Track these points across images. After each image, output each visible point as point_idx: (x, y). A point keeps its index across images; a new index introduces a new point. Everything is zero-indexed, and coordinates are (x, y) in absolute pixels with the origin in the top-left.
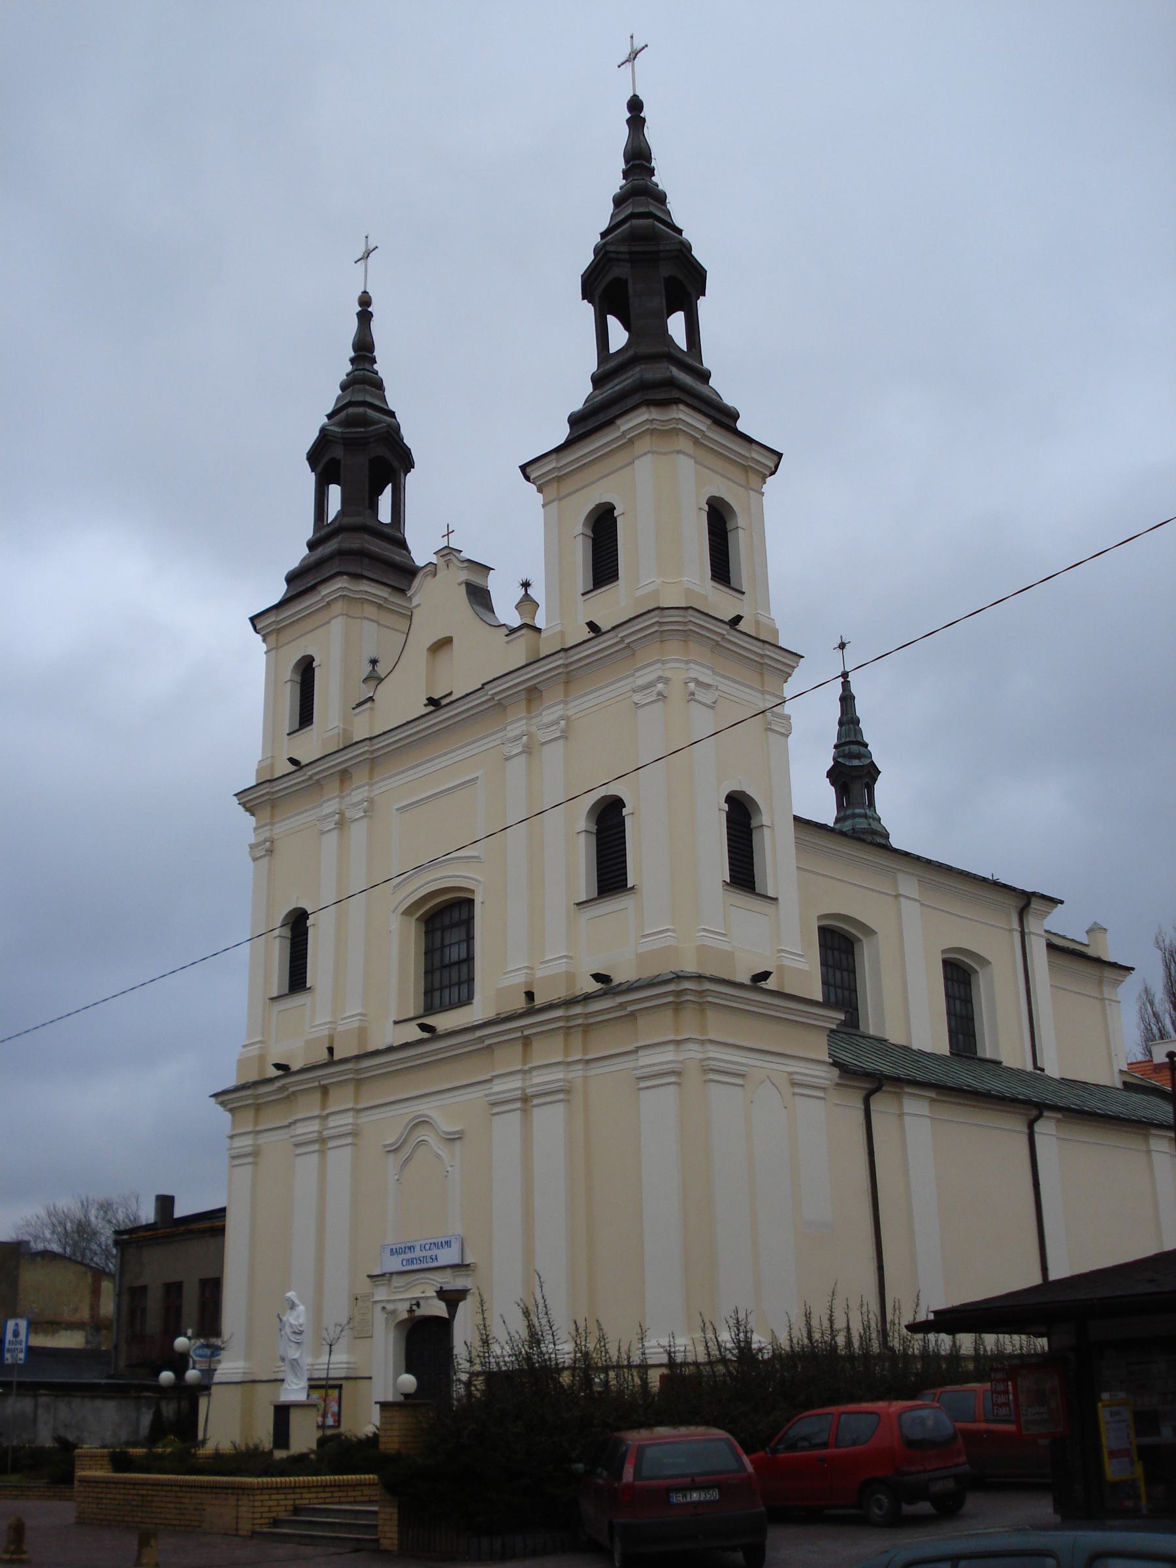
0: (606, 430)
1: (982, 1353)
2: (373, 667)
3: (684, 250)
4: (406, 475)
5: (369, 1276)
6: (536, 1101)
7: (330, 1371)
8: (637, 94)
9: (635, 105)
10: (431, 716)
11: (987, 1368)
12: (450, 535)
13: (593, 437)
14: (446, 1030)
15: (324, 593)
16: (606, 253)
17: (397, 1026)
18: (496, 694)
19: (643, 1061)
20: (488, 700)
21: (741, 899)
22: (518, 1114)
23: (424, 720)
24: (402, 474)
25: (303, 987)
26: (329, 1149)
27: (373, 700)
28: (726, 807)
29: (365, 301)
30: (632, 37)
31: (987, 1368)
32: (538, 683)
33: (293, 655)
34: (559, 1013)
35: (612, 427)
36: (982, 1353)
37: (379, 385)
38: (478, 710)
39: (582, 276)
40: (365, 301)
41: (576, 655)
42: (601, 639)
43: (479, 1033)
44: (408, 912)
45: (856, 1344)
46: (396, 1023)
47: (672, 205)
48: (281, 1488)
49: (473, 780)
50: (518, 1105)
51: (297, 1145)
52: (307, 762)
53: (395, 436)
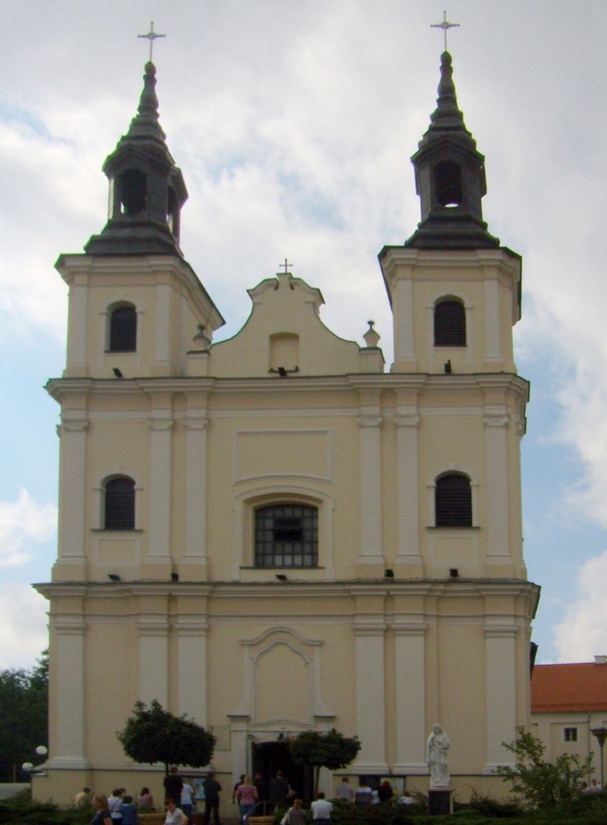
0: (467, 252)
1: (571, 786)
2: (371, 327)
5: (229, 716)
6: (398, 632)
8: (448, 51)
9: (446, 60)
10: (276, 381)
13: (454, 253)
14: (297, 580)
15: (481, 257)
17: (243, 571)
18: (482, 382)
19: (142, 621)
20: (347, 386)
22: (204, 639)
23: (248, 381)
25: (469, 525)
26: (179, 636)
27: (209, 354)
30: (445, 12)
32: (397, 388)
34: (429, 586)
35: (472, 253)
36: (571, 786)
37: (459, 116)
38: (329, 389)
41: (433, 381)
42: (120, 382)
43: (347, 587)
44: (249, 501)
46: (241, 568)
49: (321, 432)
50: (81, 632)
51: (141, 629)
52: (458, 372)
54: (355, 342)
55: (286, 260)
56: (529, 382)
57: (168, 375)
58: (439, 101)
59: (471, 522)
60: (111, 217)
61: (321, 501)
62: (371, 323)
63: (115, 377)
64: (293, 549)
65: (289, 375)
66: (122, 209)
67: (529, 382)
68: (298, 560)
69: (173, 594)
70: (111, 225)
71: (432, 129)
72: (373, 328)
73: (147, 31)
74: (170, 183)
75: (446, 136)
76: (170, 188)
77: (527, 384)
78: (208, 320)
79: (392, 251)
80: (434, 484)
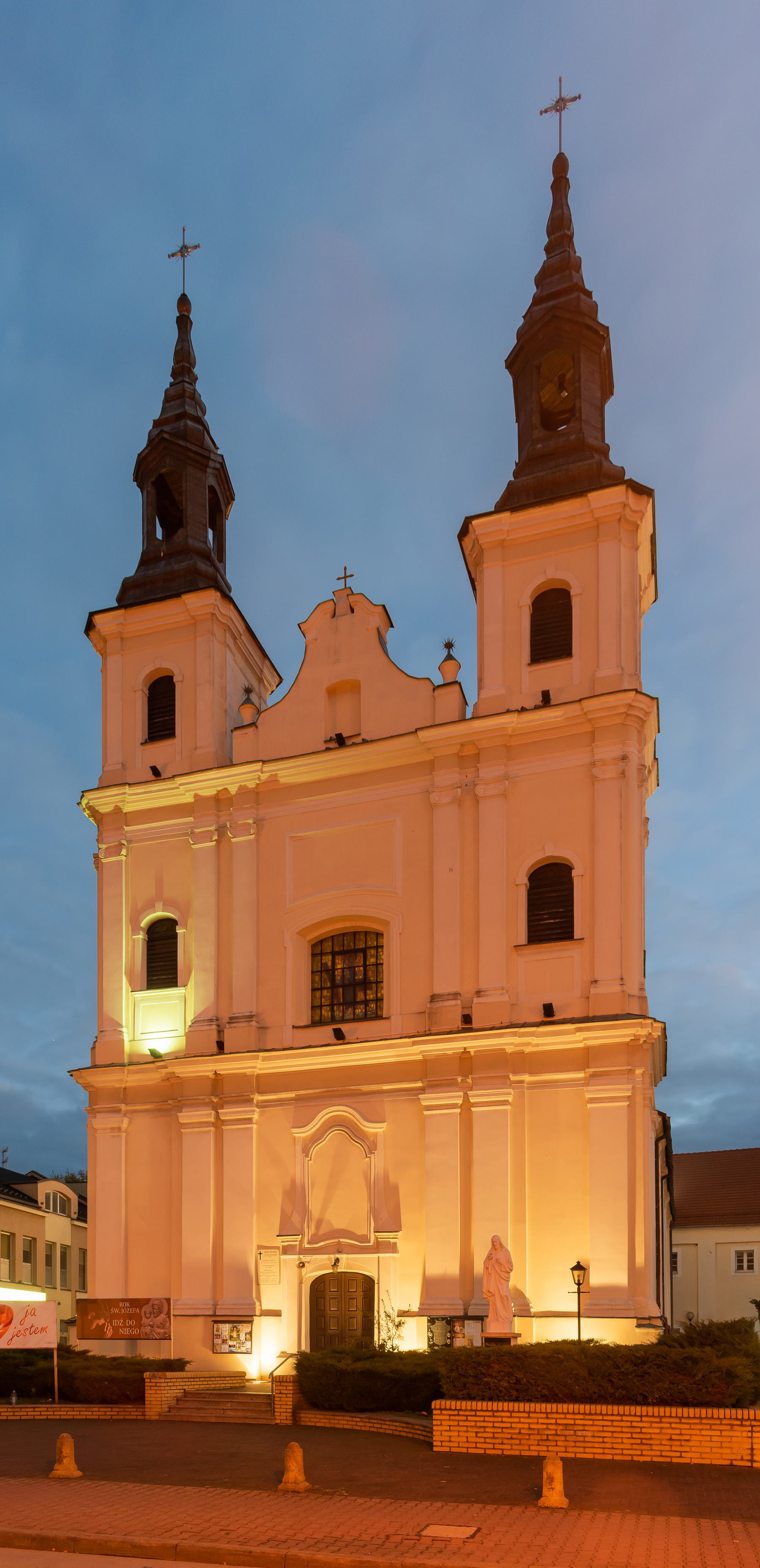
12: (347, 579)
17: (296, 1031)
44: (302, 933)
54: (428, 679)
55: (345, 569)
56: (657, 699)
57: (457, 720)
58: (548, 249)
59: (572, 932)
60: (532, 612)
61: (386, 923)
63: (153, 778)
64: (374, 983)
65: (349, 742)
66: (159, 534)
67: (657, 699)
68: (349, 1013)
69: (218, 1072)
70: (146, 561)
71: (537, 300)
72: (451, 653)
73: (193, 254)
74: (211, 481)
75: (553, 307)
76: (212, 489)
77: (656, 701)
78: (260, 680)
79: (475, 522)
80: (525, 880)
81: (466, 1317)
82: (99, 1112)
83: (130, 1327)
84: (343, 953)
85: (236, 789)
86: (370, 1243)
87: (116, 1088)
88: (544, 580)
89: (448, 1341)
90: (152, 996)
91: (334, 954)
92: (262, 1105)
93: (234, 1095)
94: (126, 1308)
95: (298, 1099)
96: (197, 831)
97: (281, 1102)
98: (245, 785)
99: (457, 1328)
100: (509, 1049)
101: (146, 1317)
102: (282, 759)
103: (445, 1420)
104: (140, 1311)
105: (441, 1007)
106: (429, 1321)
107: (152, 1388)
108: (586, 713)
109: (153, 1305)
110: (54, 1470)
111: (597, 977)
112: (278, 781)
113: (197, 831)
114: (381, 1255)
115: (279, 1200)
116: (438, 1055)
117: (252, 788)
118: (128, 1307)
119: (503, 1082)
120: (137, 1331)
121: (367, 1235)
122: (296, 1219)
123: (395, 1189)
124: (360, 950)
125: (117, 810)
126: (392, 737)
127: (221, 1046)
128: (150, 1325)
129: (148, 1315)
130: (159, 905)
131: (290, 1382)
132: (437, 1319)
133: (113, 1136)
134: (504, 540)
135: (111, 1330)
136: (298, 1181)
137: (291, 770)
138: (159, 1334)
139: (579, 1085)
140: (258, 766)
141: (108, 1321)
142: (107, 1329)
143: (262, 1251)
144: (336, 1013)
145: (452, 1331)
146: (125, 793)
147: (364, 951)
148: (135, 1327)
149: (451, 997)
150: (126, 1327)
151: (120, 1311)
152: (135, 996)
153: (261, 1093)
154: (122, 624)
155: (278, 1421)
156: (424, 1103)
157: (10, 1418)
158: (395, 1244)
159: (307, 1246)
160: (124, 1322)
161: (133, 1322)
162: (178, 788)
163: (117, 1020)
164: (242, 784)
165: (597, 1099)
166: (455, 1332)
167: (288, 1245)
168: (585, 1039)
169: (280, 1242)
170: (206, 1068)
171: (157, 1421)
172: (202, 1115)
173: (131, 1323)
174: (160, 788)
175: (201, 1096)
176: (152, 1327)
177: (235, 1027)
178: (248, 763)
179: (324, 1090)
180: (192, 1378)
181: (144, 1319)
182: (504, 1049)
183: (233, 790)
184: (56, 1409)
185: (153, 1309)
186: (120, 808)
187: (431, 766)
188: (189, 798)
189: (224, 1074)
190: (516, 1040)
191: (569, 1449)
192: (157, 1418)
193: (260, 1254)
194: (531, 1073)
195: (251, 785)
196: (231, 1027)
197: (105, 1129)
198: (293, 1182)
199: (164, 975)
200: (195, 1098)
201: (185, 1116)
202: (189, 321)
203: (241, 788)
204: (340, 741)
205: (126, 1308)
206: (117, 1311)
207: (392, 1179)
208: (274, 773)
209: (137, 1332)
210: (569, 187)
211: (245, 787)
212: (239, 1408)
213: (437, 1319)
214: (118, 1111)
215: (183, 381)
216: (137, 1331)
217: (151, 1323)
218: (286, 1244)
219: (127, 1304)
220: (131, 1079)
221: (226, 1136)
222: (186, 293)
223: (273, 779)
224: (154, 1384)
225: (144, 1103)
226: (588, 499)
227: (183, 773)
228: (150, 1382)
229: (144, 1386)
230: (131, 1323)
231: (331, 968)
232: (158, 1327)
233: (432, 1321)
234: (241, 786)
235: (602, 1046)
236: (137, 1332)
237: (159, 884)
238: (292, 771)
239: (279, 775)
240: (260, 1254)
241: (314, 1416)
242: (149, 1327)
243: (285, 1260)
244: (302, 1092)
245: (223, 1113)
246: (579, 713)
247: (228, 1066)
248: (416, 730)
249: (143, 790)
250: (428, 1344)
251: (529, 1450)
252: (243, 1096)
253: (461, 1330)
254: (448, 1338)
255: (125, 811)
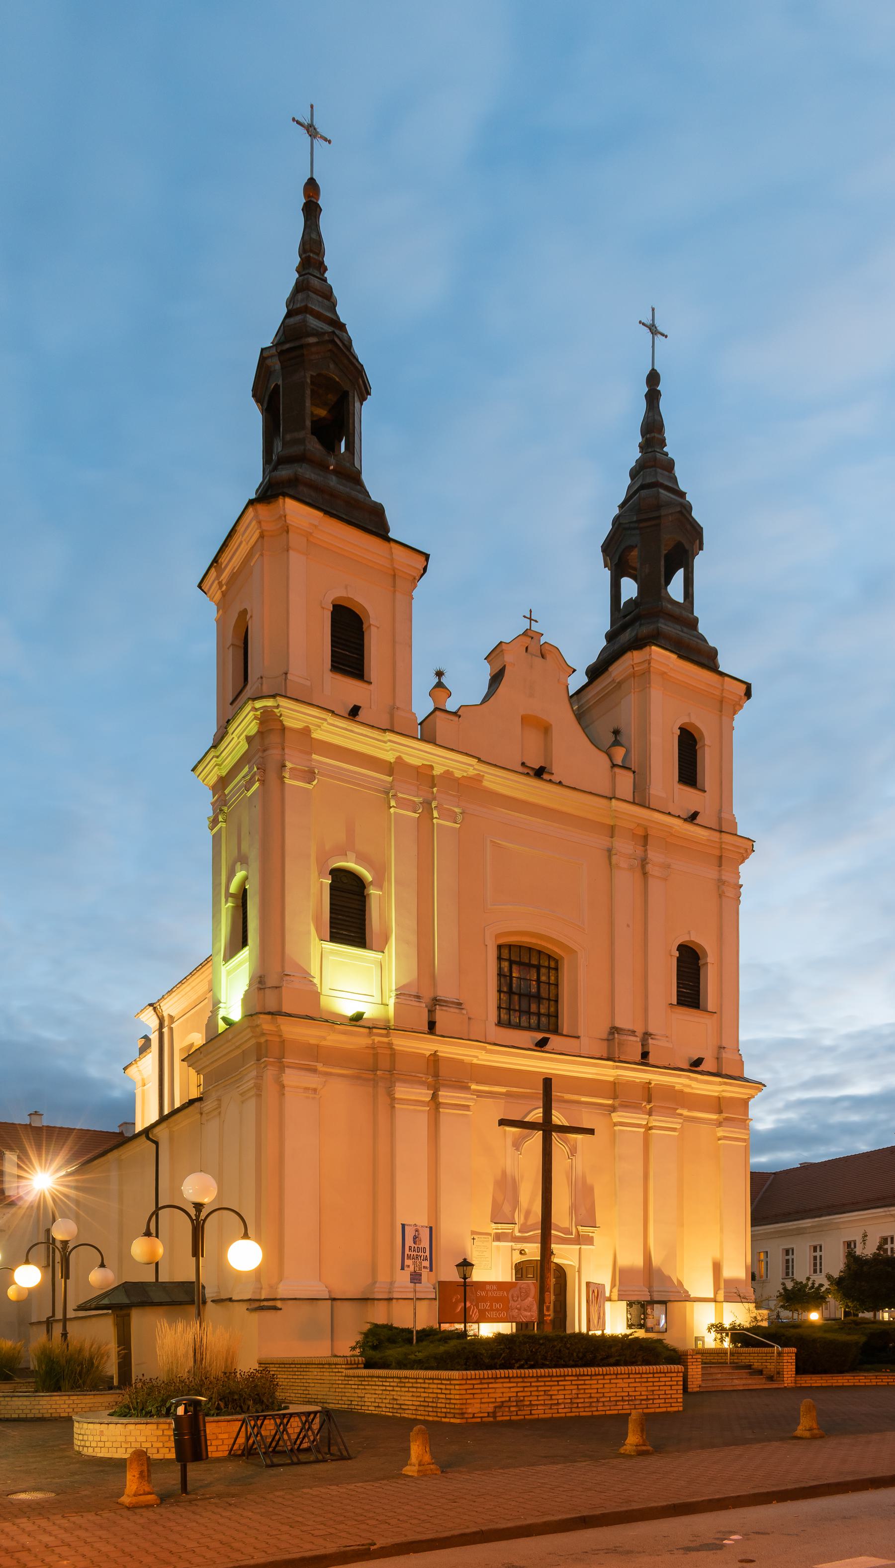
3: (685, 512)
4: (362, 404)
7: (69, 1326)
11: (598, 1355)
16: (620, 524)
21: (687, 1015)
24: (357, 404)
28: (677, 954)
29: (311, 187)
31: (598, 1355)
33: (236, 609)
39: (602, 547)
40: (311, 187)
45: (218, 1365)
47: (678, 471)
48: (712, 1353)
53: (348, 353)
54: (461, 706)
62: (439, 674)
72: (618, 739)
81: (652, 1302)
82: (288, 1067)
83: (497, 1310)
84: (520, 963)
85: (442, 771)
86: (572, 1235)
87: (309, 1044)
88: (688, 721)
89: (642, 1322)
90: (353, 954)
91: (511, 963)
92: (480, 1094)
93: (454, 1080)
94: (494, 1290)
95: (508, 1095)
96: (400, 795)
97: (491, 1095)
98: (452, 772)
99: (649, 1311)
100: (678, 1087)
101: (514, 1301)
102: (495, 766)
103: (534, 1391)
104: (508, 1294)
105: (627, 1040)
106: (628, 1305)
107: (694, 1363)
108: (721, 842)
109: (520, 1288)
110: (407, 1465)
111: (724, 1045)
112: (481, 781)
113: (400, 795)
114: (583, 1247)
115: (491, 1188)
116: (628, 1081)
117: (457, 777)
118: (495, 1290)
119: (671, 1112)
120: (504, 1314)
121: (569, 1228)
122: (507, 1208)
123: (591, 1189)
124: (533, 966)
125: (306, 732)
126: (591, 793)
127: (432, 1026)
128: (517, 1309)
129: (515, 1299)
130: (351, 855)
131: (792, 1353)
132: (634, 1303)
133: (307, 1098)
134: (665, 673)
135: (477, 1313)
136: (508, 1171)
137: (498, 778)
138: (526, 1317)
139: (712, 1124)
140: (474, 761)
141: (474, 1304)
142: (472, 1313)
143: (476, 1237)
144: (512, 1017)
145: (645, 1313)
146: (325, 720)
147: (538, 968)
148: (502, 1310)
149: (629, 1033)
150: (494, 1310)
151: (487, 1293)
152: (323, 945)
153: (478, 1083)
154: (316, 526)
155: (786, 1385)
156: (615, 1120)
157: (845, 1384)
158: (592, 1237)
159: (518, 1234)
160: (491, 1306)
161: (500, 1306)
162: (385, 742)
163: (306, 969)
164: (451, 770)
165: (731, 1137)
166: (647, 1314)
167: (502, 1232)
168: (723, 1091)
169: (493, 1228)
170: (426, 1046)
171: (697, 1393)
172: (421, 1093)
173: (498, 1306)
174: (364, 732)
175: (418, 1073)
176: (519, 1310)
177: (446, 1011)
178: (467, 754)
179: (534, 1091)
180: (277, 1364)
181: (511, 1302)
182: (674, 1087)
183: (438, 771)
184: (839, 1378)
185: (521, 1292)
186: (310, 731)
187: (612, 831)
188: (390, 757)
189: (397, 1050)
190: (686, 1081)
191: (560, 1411)
192: (698, 1389)
193: (474, 1239)
194: (690, 1109)
195: (458, 774)
196: (442, 1010)
197: (297, 1087)
198: (504, 1173)
199: (346, 930)
200: (413, 1074)
201: (402, 1091)
202: (318, 209)
203: (447, 772)
204: (539, 773)
205: (494, 1290)
206: (483, 1294)
207: (589, 1181)
208: (482, 774)
209: (504, 1315)
210: (661, 395)
211: (452, 773)
212: (727, 1377)
213: (634, 1303)
214: (314, 1071)
215: (654, 451)
216: (504, 1314)
217: (518, 1306)
218: (500, 1231)
219: (495, 1287)
220: (333, 1039)
221: (443, 1119)
222: (655, 368)
223: (478, 779)
224: (695, 1360)
225: (342, 1067)
226: (724, 680)
227: (603, 794)
228: (692, 1358)
229: (796, 1359)
230: (498, 1306)
231: (508, 974)
232: (525, 1310)
233: (630, 1304)
234: (448, 770)
235: (731, 1098)
236: (504, 1315)
237: (350, 832)
238: (499, 780)
239: (485, 778)
240: (474, 1239)
241: (810, 1379)
242: (517, 1311)
243: (498, 1247)
244: (515, 1089)
245: (443, 1096)
246: (717, 840)
247: (449, 1050)
248: (386, 729)
249: (515, 779)
250: (628, 1324)
251: (531, 1414)
252: (464, 1082)
253: (652, 1312)
254: (642, 1319)
255: (312, 736)
